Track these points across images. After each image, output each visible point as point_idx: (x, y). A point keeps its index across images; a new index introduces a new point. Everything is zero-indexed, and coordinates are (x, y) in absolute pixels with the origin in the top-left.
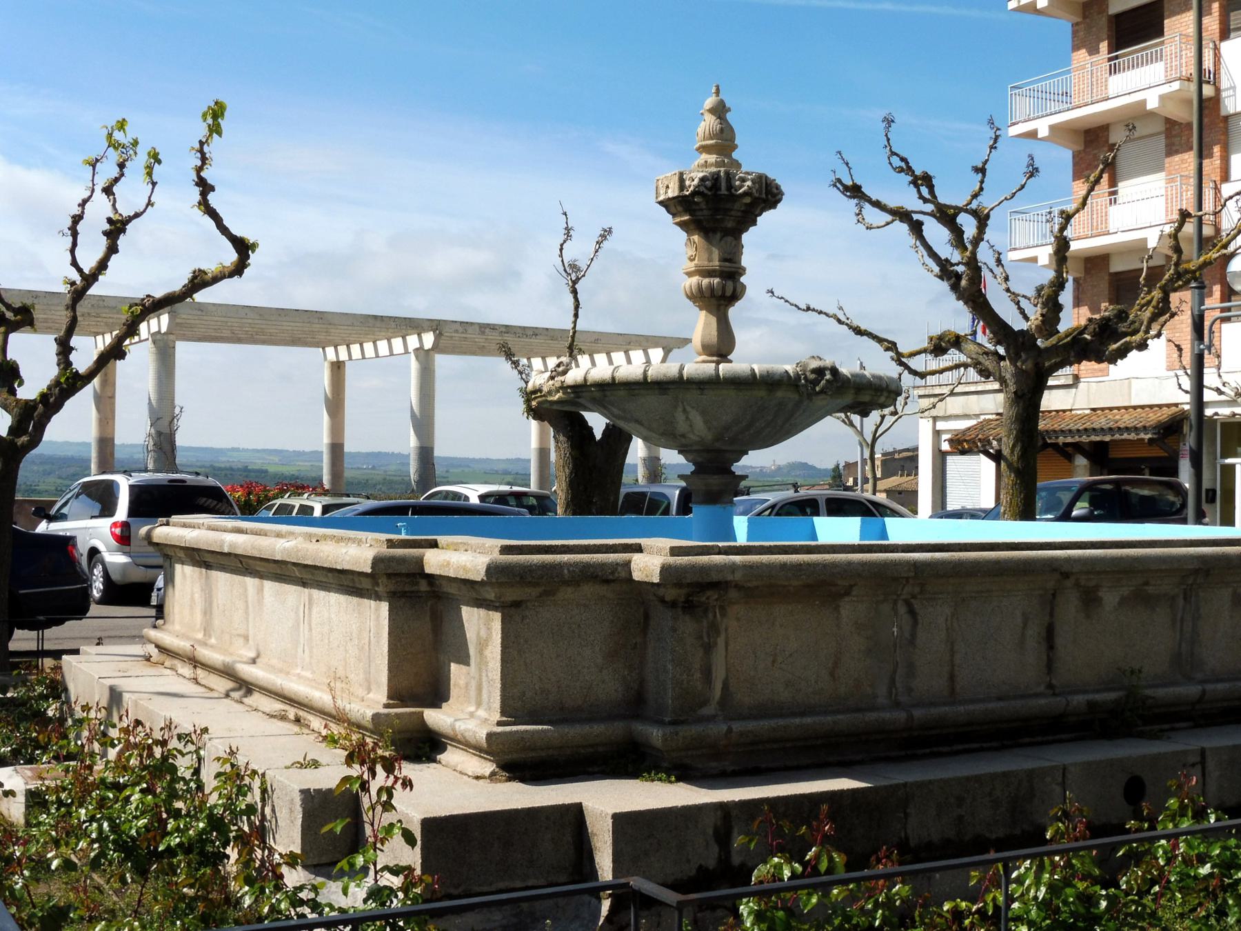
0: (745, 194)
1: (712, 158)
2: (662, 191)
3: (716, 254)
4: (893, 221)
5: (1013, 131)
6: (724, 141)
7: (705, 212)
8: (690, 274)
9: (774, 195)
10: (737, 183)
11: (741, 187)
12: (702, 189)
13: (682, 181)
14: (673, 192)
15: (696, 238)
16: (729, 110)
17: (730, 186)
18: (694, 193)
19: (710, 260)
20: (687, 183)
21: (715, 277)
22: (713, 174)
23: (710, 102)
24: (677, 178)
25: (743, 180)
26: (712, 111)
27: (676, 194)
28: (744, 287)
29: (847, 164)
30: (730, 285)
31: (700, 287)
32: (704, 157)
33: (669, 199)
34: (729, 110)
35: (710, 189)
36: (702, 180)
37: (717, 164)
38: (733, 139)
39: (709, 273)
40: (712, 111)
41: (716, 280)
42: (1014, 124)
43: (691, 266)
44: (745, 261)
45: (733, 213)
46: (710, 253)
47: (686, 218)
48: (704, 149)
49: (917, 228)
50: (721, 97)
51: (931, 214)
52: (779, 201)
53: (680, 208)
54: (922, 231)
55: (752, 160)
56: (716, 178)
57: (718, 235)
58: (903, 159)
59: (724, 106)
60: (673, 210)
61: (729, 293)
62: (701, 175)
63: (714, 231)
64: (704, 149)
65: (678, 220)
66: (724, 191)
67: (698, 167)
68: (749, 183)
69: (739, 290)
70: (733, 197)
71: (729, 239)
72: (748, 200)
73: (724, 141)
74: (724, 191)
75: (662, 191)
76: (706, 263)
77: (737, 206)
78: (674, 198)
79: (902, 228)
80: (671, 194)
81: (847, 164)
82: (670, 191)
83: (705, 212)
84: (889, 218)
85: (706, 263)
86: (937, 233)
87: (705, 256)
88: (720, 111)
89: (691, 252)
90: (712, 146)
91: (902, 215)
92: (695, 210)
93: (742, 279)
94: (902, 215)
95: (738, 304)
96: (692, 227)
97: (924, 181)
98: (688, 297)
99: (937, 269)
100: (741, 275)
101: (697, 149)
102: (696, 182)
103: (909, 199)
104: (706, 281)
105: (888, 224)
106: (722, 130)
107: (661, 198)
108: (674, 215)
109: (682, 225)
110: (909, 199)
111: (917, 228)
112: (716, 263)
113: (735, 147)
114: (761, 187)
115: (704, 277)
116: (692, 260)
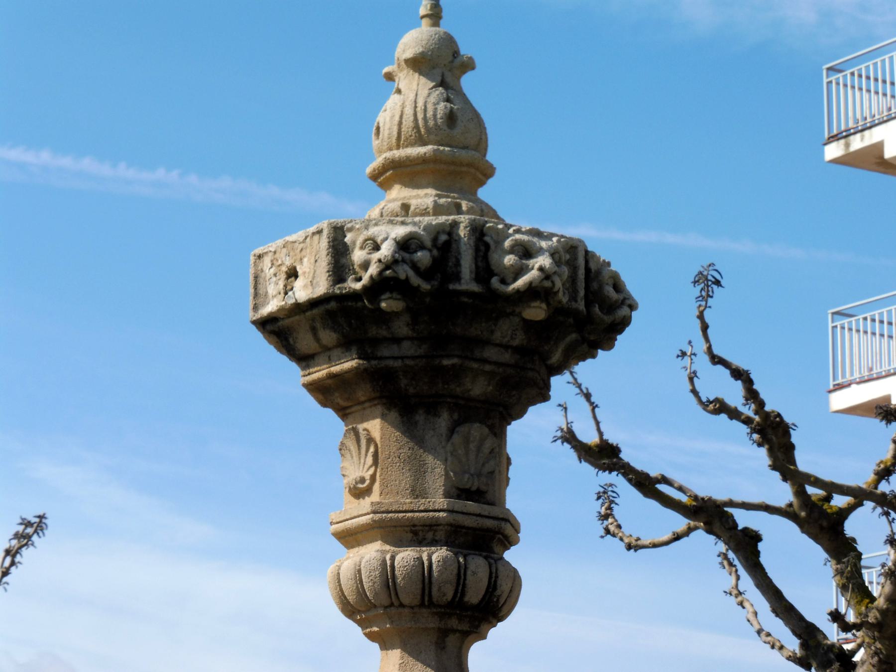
0: (532, 292)
1: (424, 197)
2: (273, 287)
3: (437, 476)
4: (689, 530)
5: (841, 400)
6: (454, 152)
7: (408, 348)
8: (350, 538)
9: (611, 307)
10: (509, 260)
11: (520, 271)
12: (404, 272)
13: (339, 251)
14: (312, 285)
15: (374, 427)
16: (468, 65)
17: (485, 270)
18: (378, 286)
19: (418, 492)
20: (358, 256)
21: (434, 543)
22: (436, 232)
23: (413, 40)
24: (323, 243)
25: (526, 252)
26: (419, 64)
27: (322, 288)
28: (515, 579)
29: (588, 396)
30: (478, 566)
31: (387, 576)
32: (398, 194)
33: (298, 308)
34: (468, 65)
35: (425, 274)
36: (405, 245)
37: (438, 210)
38: (481, 144)
39: (417, 533)
40: (419, 64)
41: (439, 555)
42: (839, 387)
43: (360, 512)
44: (515, 501)
45: (491, 353)
46: (419, 472)
47: (349, 364)
48: (394, 173)
49: (746, 546)
50: (446, 25)
51: (787, 513)
52: (622, 325)
53: (328, 337)
54: (757, 553)
55: (537, 200)
56: (443, 243)
57: (443, 421)
58: (739, 374)
59: (456, 53)
60: (305, 342)
61: (474, 595)
62: (400, 231)
63: (432, 407)
64: (394, 173)
65: (320, 373)
66: (467, 283)
67: (386, 222)
68: (544, 261)
69: (504, 586)
70: (493, 303)
71: (476, 430)
72: (536, 312)
73: (454, 152)
74: (467, 283)
75: (273, 287)
76: (407, 502)
77: (505, 331)
78: (313, 303)
79: (706, 545)
80: (302, 292)
81: (588, 396)
82: (298, 284)
83: (408, 348)
84: (680, 522)
85: (407, 502)
86: (794, 557)
87: (404, 480)
88: (443, 65)
89: (358, 468)
90: (423, 160)
91: (710, 515)
92: (376, 342)
93: (511, 556)
94: (710, 515)
95: (498, 632)
96: (363, 392)
97: (774, 435)
98: (349, 609)
99: (793, 644)
100: (508, 541)
101: (374, 177)
102: (386, 250)
103: (739, 472)
104: (405, 557)
105: (677, 537)
106: (451, 118)
107: (271, 307)
108: (304, 360)
109: (323, 391)
110: (739, 472)
111: (746, 546)
112: (438, 500)
113: (486, 172)
114: (573, 279)
115: (400, 543)
116: (359, 492)
